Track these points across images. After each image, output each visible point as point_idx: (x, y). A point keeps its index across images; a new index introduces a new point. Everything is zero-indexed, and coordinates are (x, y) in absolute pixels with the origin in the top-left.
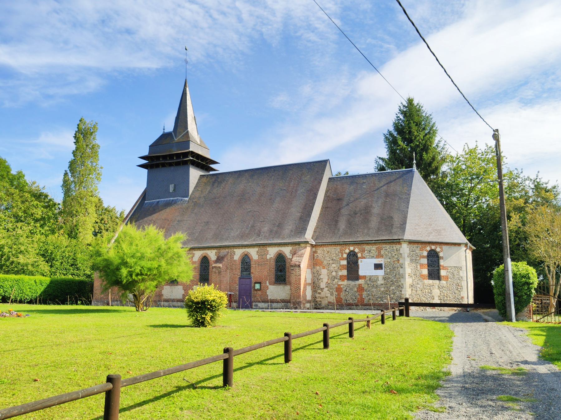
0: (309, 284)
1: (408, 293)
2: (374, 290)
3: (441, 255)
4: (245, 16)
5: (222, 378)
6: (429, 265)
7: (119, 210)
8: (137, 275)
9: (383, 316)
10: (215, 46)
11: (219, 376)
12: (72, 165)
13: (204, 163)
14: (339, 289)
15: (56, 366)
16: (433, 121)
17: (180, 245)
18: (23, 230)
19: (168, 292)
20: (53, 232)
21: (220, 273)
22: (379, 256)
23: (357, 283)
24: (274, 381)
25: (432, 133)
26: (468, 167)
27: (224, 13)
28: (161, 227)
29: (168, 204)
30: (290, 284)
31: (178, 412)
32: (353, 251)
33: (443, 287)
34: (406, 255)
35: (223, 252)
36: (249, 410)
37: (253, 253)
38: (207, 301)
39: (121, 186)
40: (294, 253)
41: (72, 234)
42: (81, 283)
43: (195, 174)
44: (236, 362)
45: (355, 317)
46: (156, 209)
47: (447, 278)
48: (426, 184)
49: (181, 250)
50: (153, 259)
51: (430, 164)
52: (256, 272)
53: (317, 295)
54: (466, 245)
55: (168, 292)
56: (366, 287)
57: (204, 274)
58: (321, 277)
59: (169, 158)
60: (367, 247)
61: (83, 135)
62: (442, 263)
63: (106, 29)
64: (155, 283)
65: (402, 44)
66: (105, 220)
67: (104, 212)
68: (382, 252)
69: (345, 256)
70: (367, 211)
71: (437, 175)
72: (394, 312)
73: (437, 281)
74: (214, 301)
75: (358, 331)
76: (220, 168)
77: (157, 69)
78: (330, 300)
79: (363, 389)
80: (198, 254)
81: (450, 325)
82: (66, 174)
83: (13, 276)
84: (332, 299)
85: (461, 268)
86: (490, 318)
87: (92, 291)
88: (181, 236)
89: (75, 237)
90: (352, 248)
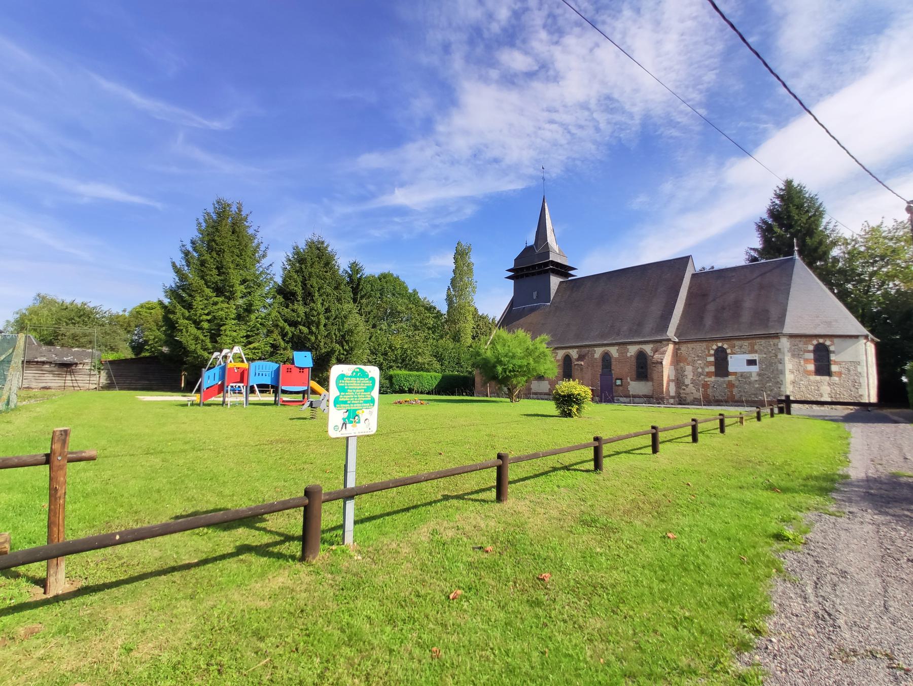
0: (673, 381)
1: (789, 390)
2: (747, 386)
3: (832, 348)
4: (602, 126)
5: (592, 463)
6: (816, 360)
7: (491, 317)
8: (510, 371)
9: (758, 413)
10: (574, 159)
11: (590, 461)
12: (453, 281)
13: (563, 270)
14: (705, 386)
15: (454, 444)
16: (820, 201)
17: (545, 346)
18: (420, 335)
19: (536, 386)
20: (442, 337)
21: (582, 370)
22: (752, 351)
23: (726, 379)
24: (643, 470)
25: (819, 214)
26: (868, 248)
27: (581, 127)
28: (527, 330)
29: (533, 310)
30: (652, 380)
31: (556, 489)
32: (721, 347)
33: (834, 384)
34: (786, 350)
35: (585, 350)
36: (620, 493)
37: (614, 351)
38: (573, 395)
39: (493, 298)
40: (655, 351)
41: (456, 338)
42: (465, 378)
43: (555, 281)
44: (606, 449)
45: (726, 414)
46: (521, 314)
47: (839, 374)
48: (811, 272)
49: (546, 350)
50: (523, 358)
51: (816, 249)
52: (616, 369)
53: (682, 391)
54: (866, 337)
55: (536, 386)
56: (737, 383)
57: (567, 370)
58: (686, 373)
59: (532, 268)
60: (737, 343)
61: (461, 255)
62: (833, 357)
63: (478, 162)
64: (525, 379)
65: (781, 119)
66: (482, 325)
67: (480, 319)
68: (756, 347)
69: (712, 352)
70: (737, 306)
71: (825, 261)
72: (772, 410)
73: (827, 378)
74: (579, 394)
75: (730, 427)
76: (579, 274)
77: (522, 190)
78: (697, 397)
79: (740, 484)
80: (561, 354)
81: (846, 426)
82: (449, 289)
83: (415, 373)
84: (699, 395)
85: (859, 363)
86: (901, 419)
87: (474, 385)
88: (545, 337)
89: (458, 341)
90: (720, 344)
